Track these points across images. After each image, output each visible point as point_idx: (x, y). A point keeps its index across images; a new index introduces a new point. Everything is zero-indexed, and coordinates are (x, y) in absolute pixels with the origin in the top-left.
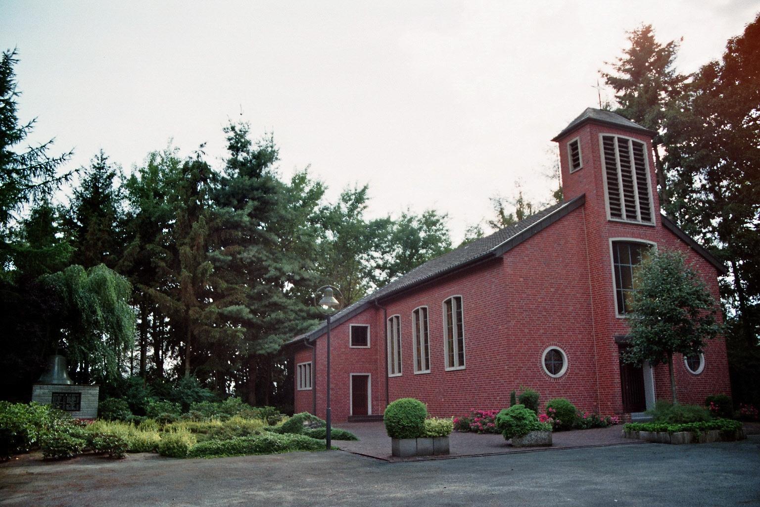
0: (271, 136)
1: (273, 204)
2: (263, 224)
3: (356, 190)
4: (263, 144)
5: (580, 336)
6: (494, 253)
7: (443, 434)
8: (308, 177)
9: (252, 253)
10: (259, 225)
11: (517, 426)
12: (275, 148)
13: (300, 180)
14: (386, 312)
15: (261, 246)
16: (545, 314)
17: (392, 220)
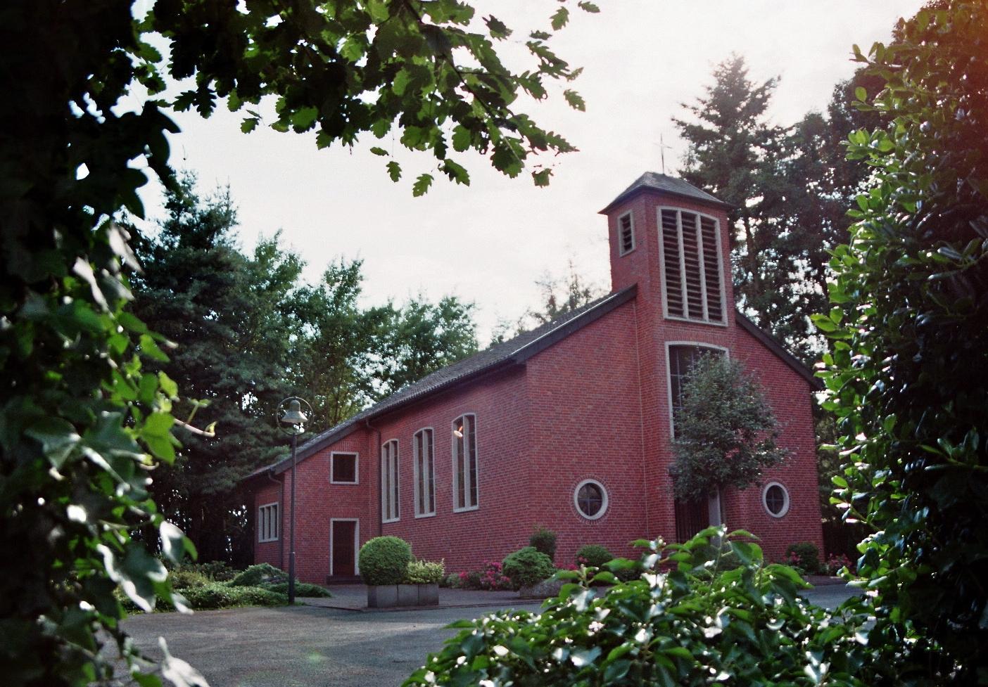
0: (226, 190)
1: (227, 285)
2: (214, 313)
3: (343, 267)
4: (215, 201)
5: (625, 467)
6: (515, 358)
7: (431, 580)
8: (279, 248)
9: (197, 354)
10: (209, 314)
11: (526, 572)
12: (232, 208)
13: (266, 252)
14: (380, 436)
15: (210, 344)
16: (579, 437)
17: (395, 308)
